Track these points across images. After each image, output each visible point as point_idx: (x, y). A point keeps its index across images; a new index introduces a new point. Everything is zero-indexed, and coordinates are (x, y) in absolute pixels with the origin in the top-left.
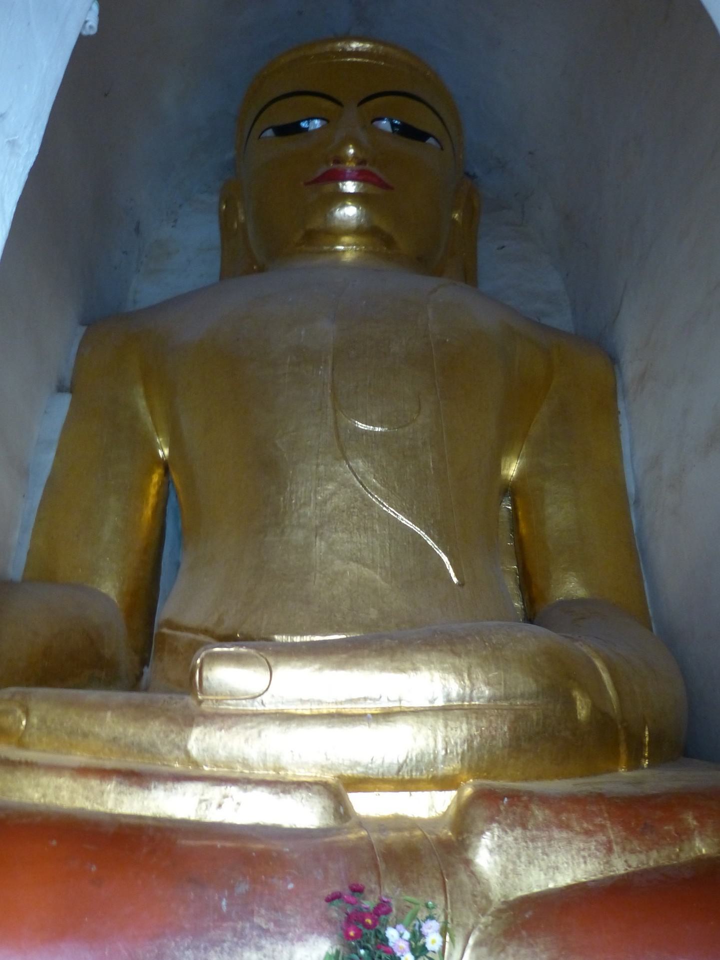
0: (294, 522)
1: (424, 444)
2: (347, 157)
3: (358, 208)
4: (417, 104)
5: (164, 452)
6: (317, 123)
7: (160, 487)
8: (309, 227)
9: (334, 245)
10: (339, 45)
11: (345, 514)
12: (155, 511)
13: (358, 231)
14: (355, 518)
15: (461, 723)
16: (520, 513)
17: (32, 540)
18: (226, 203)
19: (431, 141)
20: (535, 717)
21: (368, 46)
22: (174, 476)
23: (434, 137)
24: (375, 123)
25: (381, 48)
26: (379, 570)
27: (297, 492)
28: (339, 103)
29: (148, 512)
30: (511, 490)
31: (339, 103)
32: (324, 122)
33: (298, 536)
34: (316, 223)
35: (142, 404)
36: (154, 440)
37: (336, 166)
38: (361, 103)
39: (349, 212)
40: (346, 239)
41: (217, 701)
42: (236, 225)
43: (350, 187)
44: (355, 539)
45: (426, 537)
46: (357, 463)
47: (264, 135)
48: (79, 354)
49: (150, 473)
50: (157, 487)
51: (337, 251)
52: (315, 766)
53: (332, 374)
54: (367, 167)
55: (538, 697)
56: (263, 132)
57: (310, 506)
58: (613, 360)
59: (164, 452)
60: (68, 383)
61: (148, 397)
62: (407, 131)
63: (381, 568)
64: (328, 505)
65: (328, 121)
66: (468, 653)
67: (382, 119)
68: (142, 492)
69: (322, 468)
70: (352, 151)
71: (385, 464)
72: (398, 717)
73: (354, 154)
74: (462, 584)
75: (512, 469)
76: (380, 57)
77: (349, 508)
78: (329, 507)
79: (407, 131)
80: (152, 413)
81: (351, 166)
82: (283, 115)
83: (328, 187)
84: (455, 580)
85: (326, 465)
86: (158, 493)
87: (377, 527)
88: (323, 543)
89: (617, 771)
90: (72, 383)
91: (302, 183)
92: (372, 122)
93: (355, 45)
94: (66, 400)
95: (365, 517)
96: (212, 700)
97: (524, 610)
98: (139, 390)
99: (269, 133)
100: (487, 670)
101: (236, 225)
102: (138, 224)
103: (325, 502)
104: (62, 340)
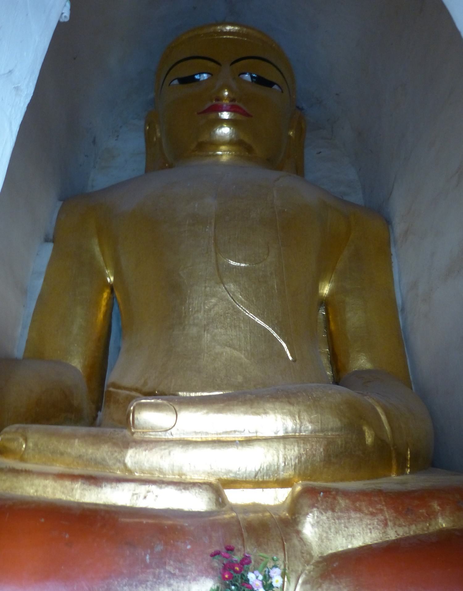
1: (271, 274)
3: (230, 129)
5: (111, 279)
6: (205, 76)
7: (108, 301)
8: (200, 140)
10: (219, 27)
11: (222, 317)
12: (105, 316)
15: (294, 446)
18: (149, 125)
19: (275, 87)
21: (237, 28)
24: (241, 76)
27: (193, 304)
28: (219, 64)
30: (325, 302)
31: (219, 64)
32: (210, 76)
34: (205, 138)
35: (97, 249)
36: (105, 272)
37: (217, 103)
39: (225, 131)
40: (223, 148)
41: (143, 432)
42: (155, 139)
43: (225, 115)
44: (228, 333)
45: (272, 332)
46: (230, 286)
48: (58, 219)
49: (101, 292)
50: (106, 301)
51: (218, 155)
54: (236, 103)
55: (341, 430)
57: (200, 312)
59: (111, 279)
60: (51, 237)
61: (101, 245)
63: (244, 350)
64: (212, 312)
65: (212, 75)
66: (298, 403)
69: (208, 289)
70: (226, 93)
73: (228, 95)
74: (294, 360)
75: (325, 290)
76: (243, 35)
77: (225, 314)
78: (212, 313)
80: (103, 255)
81: (226, 102)
82: (184, 71)
83: (212, 116)
85: (211, 287)
86: (107, 304)
87: (242, 325)
88: (209, 335)
91: (196, 113)
92: (239, 75)
93: (228, 28)
95: (235, 319)
96: (140, 432)
97: (333, 376)
98: (95, 241)
99: (176, 82)
101: (155, 139)
103: (210, 310)
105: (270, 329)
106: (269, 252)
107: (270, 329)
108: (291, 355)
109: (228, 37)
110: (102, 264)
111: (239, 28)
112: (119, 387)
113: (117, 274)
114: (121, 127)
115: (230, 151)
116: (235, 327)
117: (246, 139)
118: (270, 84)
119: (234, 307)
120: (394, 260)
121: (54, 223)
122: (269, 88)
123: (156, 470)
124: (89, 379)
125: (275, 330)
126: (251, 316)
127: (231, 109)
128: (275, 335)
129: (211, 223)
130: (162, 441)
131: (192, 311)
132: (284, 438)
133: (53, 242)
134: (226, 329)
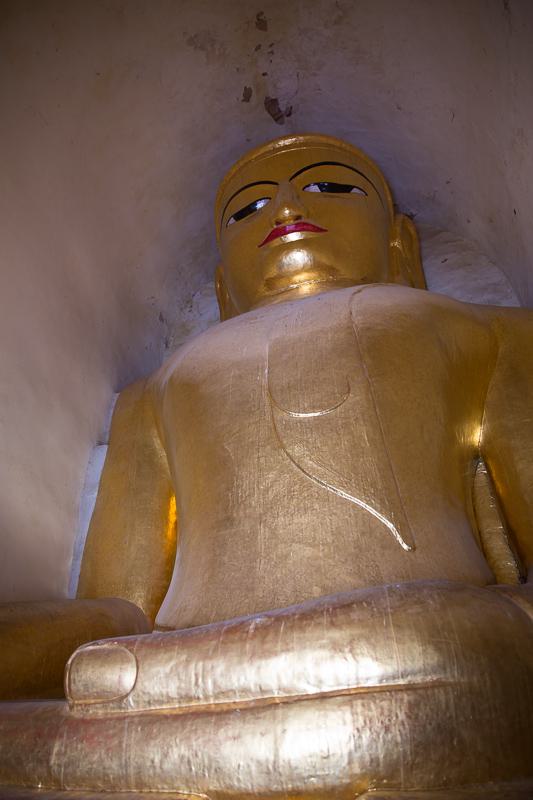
1: (356, 419)
3: (309, 253)
4: (338, 167)
8: (267, 276)
10: (270, 146)
15: (344, 713)
16: (494, 475)
17: (82, 566)
19: (355, 190)
20: (442, 698)
25: (301, 138)
26: (321, 547)
28: (276, 184)
30: (477, 455)
31: (276, 184)
33: (246, 526)
34: (273, 272)
41: (86, 705)
43: (294, 237)
44: (296, 521)
45: (369, 508)
46: (293, 450)
51: (292, 289)
54: (303, 220)
55: (445, 669)
63: (323, 544)
66: (350, 623)
69: (262, 460)
70: (287, 212)
72: (308, 707)
74: (414, 549)
75: (477, 436)
76: (301, 145)
77: (289, 492)
78: (271, 495)
82: (241, 203)
83: (276, 242)
87: (316, 506)
88: (267, 529)
89: (293, 788)
93: (282, 143)
94: (102, 453)
95: (305, 498)
96: (81, 705)
97: (517, 567)
99: (232, 220)
100: (373, 640)
103: (267, 490)
105: (362, 504)
106: (349, 389)
107: (362, 504)
108: (405, 541)
116: (306, 510)
117: (324, 260)
118: (347, 189)
119: (302, 480)
121: (109, 424)
123: (99, 778)
125: (371, 505)
126: (346, 496)
127: (298, 228)
128: (374, 512)
130: (166, 717)
132: (381, 691)
133: (108, 444)
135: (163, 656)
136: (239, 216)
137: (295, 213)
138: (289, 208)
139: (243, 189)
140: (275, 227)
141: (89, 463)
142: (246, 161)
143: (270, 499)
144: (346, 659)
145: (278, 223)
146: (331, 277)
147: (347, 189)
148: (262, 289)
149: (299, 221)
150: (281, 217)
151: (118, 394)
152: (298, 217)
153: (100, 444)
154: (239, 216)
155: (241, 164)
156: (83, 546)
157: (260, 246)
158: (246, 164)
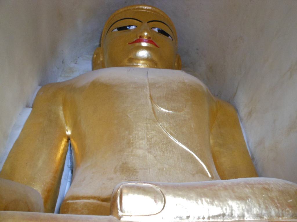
0: (138, 147)
2: (144, 35)
3: (148, 51)
5: (69, 133)
6: (134, 27)
7: (65, 146)
9: (138, 63)
11: (160, 144)
12: (62, 156)
13: (147, 59)
14: (165, 146)
18: (96, 55)
19: (170, 37)
21: (150, 8)
22: (73, 142)
23: (171, 36)
24: (153, 29)
27: (138, 134)
28: (141, 22)
29: (59, 156)
31: (141, 22)
32: (136, 27)
35: (61, 113)
36: (65, 127)
37: (140, 38)
38: (149, 22)
39: (143, 54)
40: (142, 62)
42: (99, 62)
43: (144, 44)
47: (113, 31)
48: (37, 94)
49: (61, 141)
50: (64, 146)
52: (235, 215)
53: (150, 92)
54: (151, 39)
56: (113, 30)
57: (144, 139)
58: (236, 110)
59: (69, 133)
60: (31, 103)
61: (64, 110)
62: (161, 32)
64: (153, 139)
65: (137, 27)
67: (155, 28)
68: (57, 147)
70: (146, 34)
71: (175, 125)
73: (147, 35)
79: (161, 32)
80: (65, 117)
81: (145, 38)
83: (137, 44)
84: (210, 176)
85: (150, 124)
86: (64, 149)
90: (32, 105)
91: (128, 43)
92: (152, 28)
94: (30, 110)
98: (61, 108)
99: (116, 30)
101: (99, 62)
102: (63, 60)
104: (32, 88)
109: (144, 11)
110: (64, 122)
111: (152, 8)
112: (78, 198)
113: (75, 127)
114: (78, 58)
115: (146, 64)
117: (156, 59)
118: (167, 35)
120: (243, 130)
122: (166, 37)
124: (46, 202)
127: (149, 41)
129: (147, 88)
131: (138, 139)
133: (32, 108)
134: (163, 152)
135: (62, 153)
136: (120, 29)
137: (149, 36)
138: (148, 32)
139: (111, 27)
140: (139, 38)
141: (20, 114)
142: (128, 8)
143: (153, 142)
144: (193, 202)
145: (140, 37)
146: (152, 63)
147: (167, 35)
148: (126, 61)
149: (149, 39)
150: (143, 35)
151: (40, 87)
152: (149, 38)
153: (27, 106)
154: (120, 29)
155: (126, 9)
156: (6, 156)
157: (129, 44)
158: (128, 10)
